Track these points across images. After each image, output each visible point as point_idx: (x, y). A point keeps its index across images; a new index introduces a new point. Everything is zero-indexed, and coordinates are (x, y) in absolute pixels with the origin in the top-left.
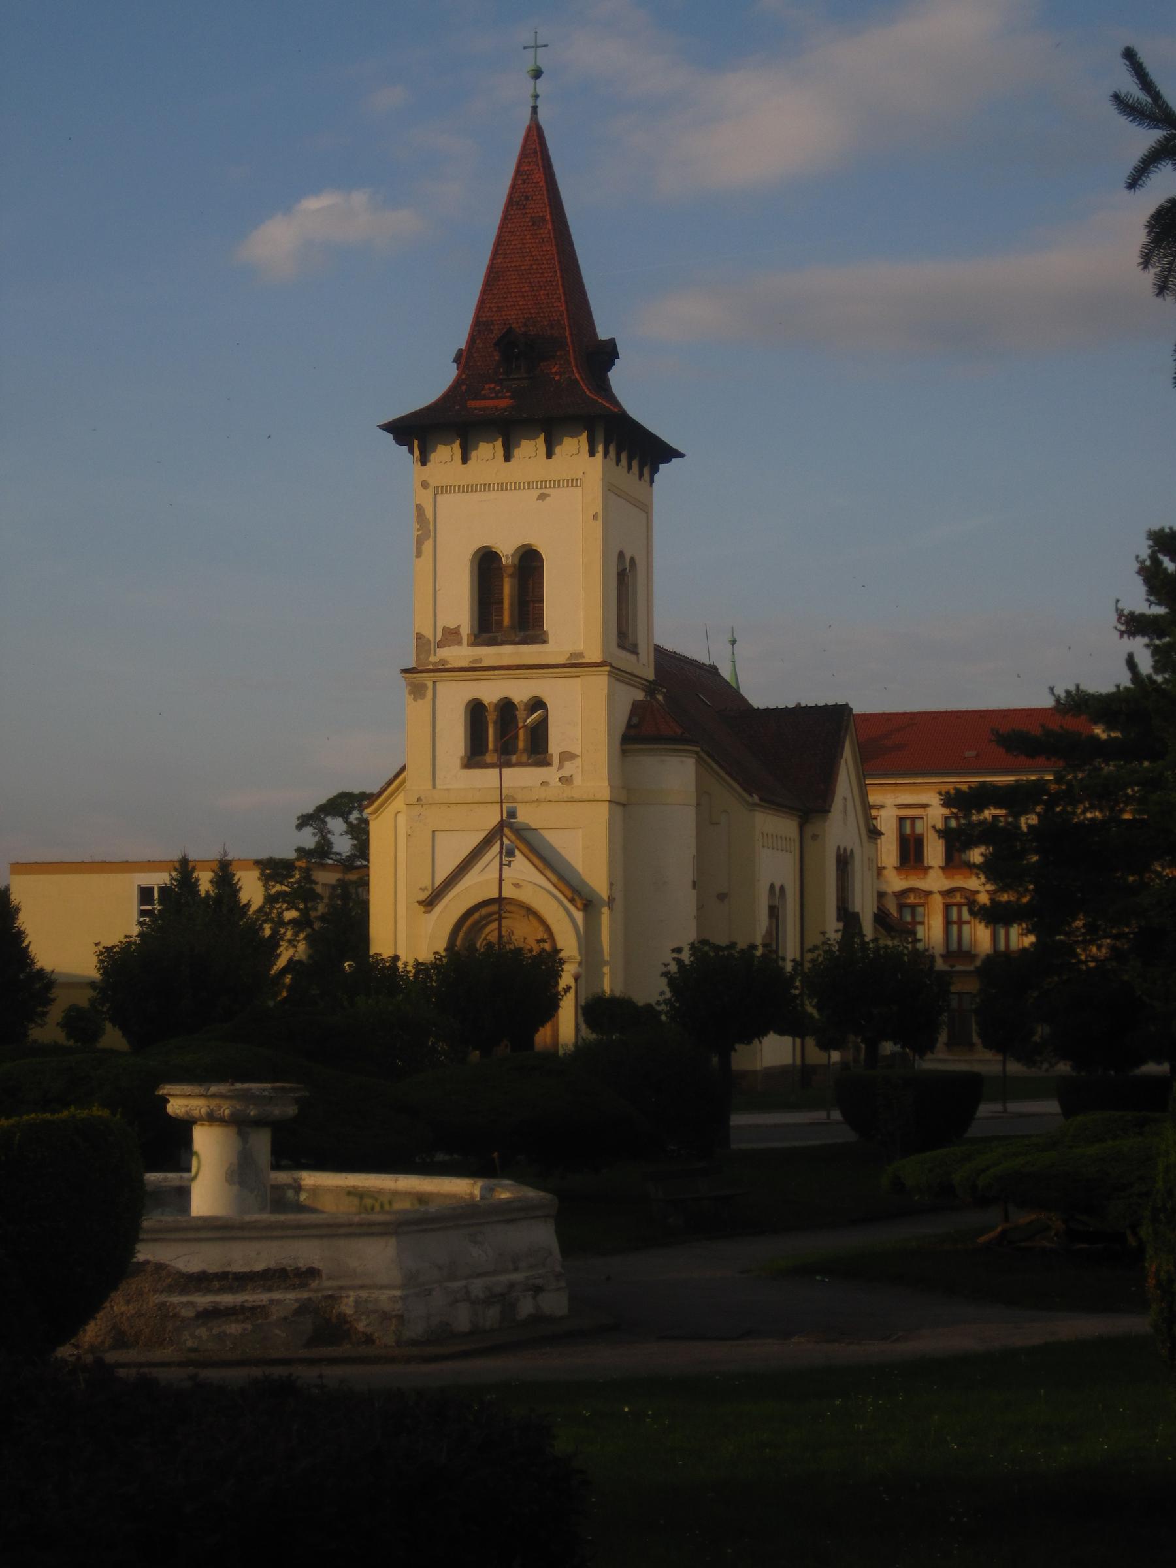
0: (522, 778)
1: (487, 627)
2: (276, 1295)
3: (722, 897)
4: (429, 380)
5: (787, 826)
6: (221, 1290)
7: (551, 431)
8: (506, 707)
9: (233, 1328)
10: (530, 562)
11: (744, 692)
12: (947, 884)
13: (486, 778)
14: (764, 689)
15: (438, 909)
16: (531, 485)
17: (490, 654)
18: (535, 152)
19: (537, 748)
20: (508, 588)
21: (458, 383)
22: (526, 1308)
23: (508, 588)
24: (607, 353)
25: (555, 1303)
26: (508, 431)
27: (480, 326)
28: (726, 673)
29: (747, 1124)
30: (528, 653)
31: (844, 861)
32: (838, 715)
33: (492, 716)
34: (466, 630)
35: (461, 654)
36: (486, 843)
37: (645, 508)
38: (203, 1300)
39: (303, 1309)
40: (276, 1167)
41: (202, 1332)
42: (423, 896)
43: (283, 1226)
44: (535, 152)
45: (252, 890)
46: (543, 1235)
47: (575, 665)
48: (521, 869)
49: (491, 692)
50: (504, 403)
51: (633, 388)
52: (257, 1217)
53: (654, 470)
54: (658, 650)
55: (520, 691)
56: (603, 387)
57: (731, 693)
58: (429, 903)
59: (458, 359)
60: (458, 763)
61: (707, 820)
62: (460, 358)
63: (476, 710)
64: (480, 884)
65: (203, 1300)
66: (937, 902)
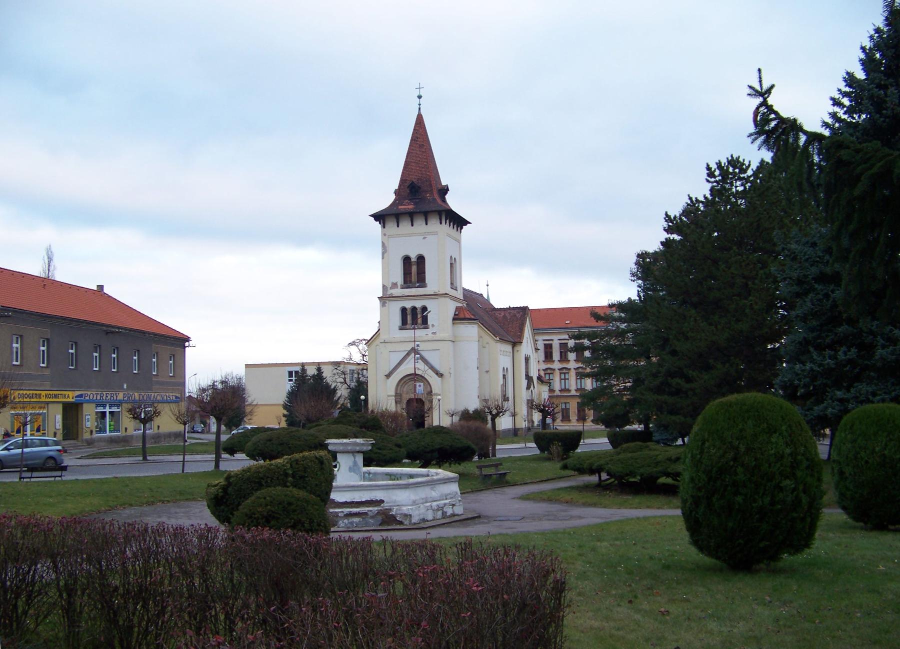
0: (421, 333)
1: (408, 282)
2: (371, 509)
3: (487, 372)
4: (386, 200)
5: (509, 348)
6: (352, 507)
7: (426, 215)
8: (414, 309)
9: (356, 520)
10: (421, 259)
11: (492, 302)
12: (561, 366)
13: (408, 334)
14: (498, 302)
15: (391, 378)
16: (420, 234)
17: (408, 292)
18: (420, 122)
19: (425, 320)
20: (414, 269)
21: (395, 200)
22: (449, 511)
23: (414, 269)
24: (445, 190)
25: (459, 510)
26: (411, 216)
27: (402, 181)
28: (485, 296)
29: (503, 450)
30: (421, 291)
31: (527, 359)
32: (524, 310)
33: (409, 312)
34: (400, 280)
35: (398, 292)
36: (408, 354)
37: (459, 241)
38: (347, 510)
39: (379, 513)
40: (365, 465)
41: (346, 521)
42: (387, 373)
43: (370, 486)
44: (420, 122)
45: (327, 373)
46: (454, 488)
47: (436, 295)
48: (421, 365)
49: (408, 305)
50: (411, 207)
51: (453, 201)
52: (362, 483)
53: (462, 228)
54: (464, 289)
55: (418, 304)
56: (444, 201)
57: (487, 302)
58: (388, 376)
59: (395, 193)
60: (397, 328)
61: (482, 347)
62: (396, 192)
63: (404, 310)
64: (408, 368)
65: (347, 510)
66: (557, 373)
